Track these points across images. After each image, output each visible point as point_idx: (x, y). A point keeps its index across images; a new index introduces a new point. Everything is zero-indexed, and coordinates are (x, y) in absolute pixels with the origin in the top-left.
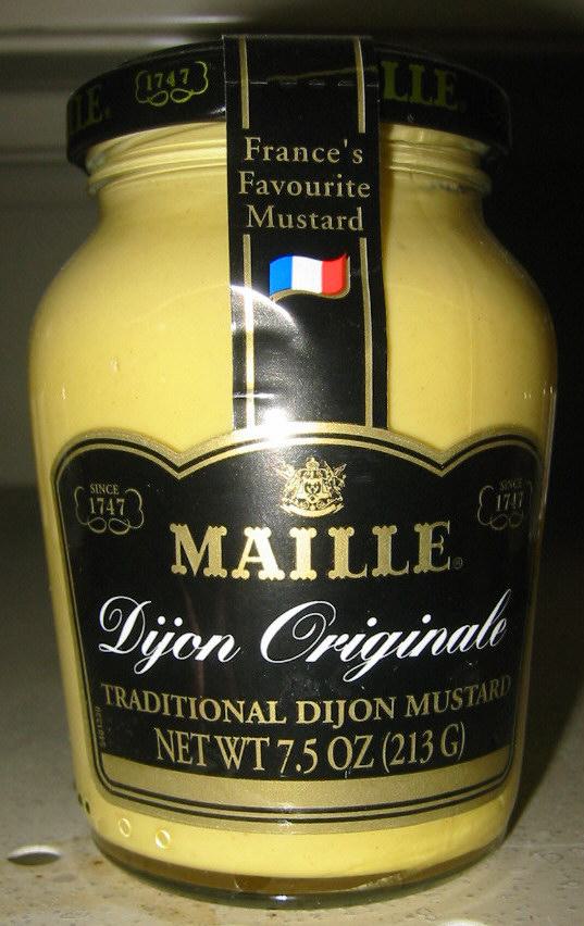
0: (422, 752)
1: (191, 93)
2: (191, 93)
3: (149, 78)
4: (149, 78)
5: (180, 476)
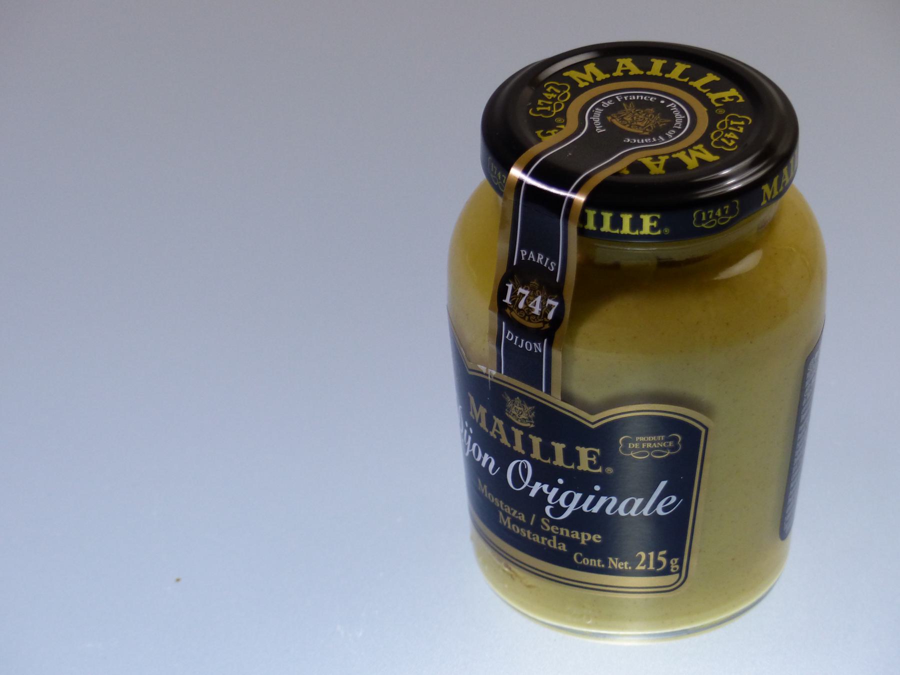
0: (658, 564)
1: (730, 218)
2: (730, 218)
3: (704, 214)
4: (704, 214)
5: (593, 427)
